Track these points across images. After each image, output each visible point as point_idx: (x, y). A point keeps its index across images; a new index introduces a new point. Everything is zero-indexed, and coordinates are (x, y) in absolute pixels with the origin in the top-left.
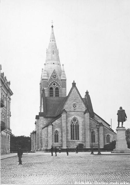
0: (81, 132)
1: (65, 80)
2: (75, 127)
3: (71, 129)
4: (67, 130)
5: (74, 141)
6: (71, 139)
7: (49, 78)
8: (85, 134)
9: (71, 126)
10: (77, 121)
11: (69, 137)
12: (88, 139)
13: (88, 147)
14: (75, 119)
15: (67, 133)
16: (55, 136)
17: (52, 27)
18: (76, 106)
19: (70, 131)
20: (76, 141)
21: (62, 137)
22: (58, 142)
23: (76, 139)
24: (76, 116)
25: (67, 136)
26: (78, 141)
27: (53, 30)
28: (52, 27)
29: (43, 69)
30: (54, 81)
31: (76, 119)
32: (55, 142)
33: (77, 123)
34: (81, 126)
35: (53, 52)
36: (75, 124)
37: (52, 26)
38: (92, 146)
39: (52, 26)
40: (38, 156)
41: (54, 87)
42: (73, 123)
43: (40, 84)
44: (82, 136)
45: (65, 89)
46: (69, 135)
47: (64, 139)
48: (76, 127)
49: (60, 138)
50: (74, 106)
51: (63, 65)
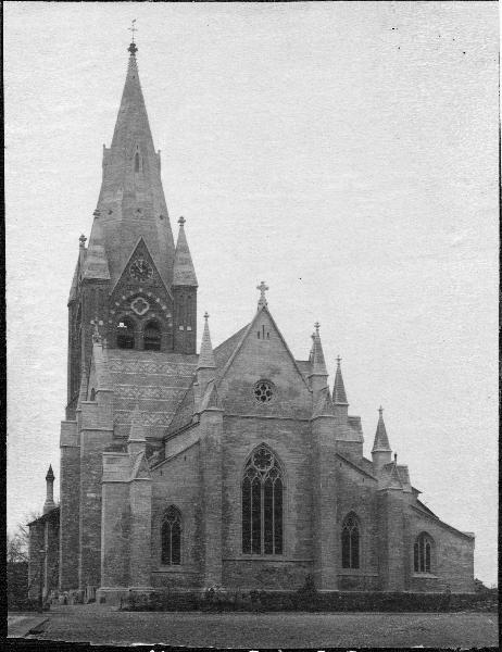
0: (294, 515)
1: (193, 289)
2: (262, 492)
3: (246, 503)
4: (225, 506)
5: (255, 557)
6: (246, 548)
7: (118, 277)
8: (312, 526)
9: (245, 487)
10: (276, 464)
11: (236, 540)
12: (329, 550)
13: (327, 588)
14: (262, 456)
15: (226, 520)
16: (165, 530)
17: (133, 49)
18: (269, 394)
19: (237, 514)
20: (269, 557)
21: (199, 535)
22: (177, 560)
23: (268, 551)
24: (267, 441)
25: (225, 536)
26: (280, 557)
27: (133, 64)
28: (133, 49)
29: (83, 239)
30: (141, 290)
31: (268, 456)
32: (165, 561)
33: (273, 472)
34: (294, 489)
35: (137, 160)
36: (263, 480)
37: (133, 45)
38: (344, 583)
39: (133, 45)
40: (33, 648)
41: (140, 318)
42: (252, 471)
43: (71, 305)
44: (298, 535)
45: (189, 329)
46: (236, 527)
47: (212, 552)
48: (268, 494)
49: (187, 546)
50: (258, 393)
51: (182, 221)
